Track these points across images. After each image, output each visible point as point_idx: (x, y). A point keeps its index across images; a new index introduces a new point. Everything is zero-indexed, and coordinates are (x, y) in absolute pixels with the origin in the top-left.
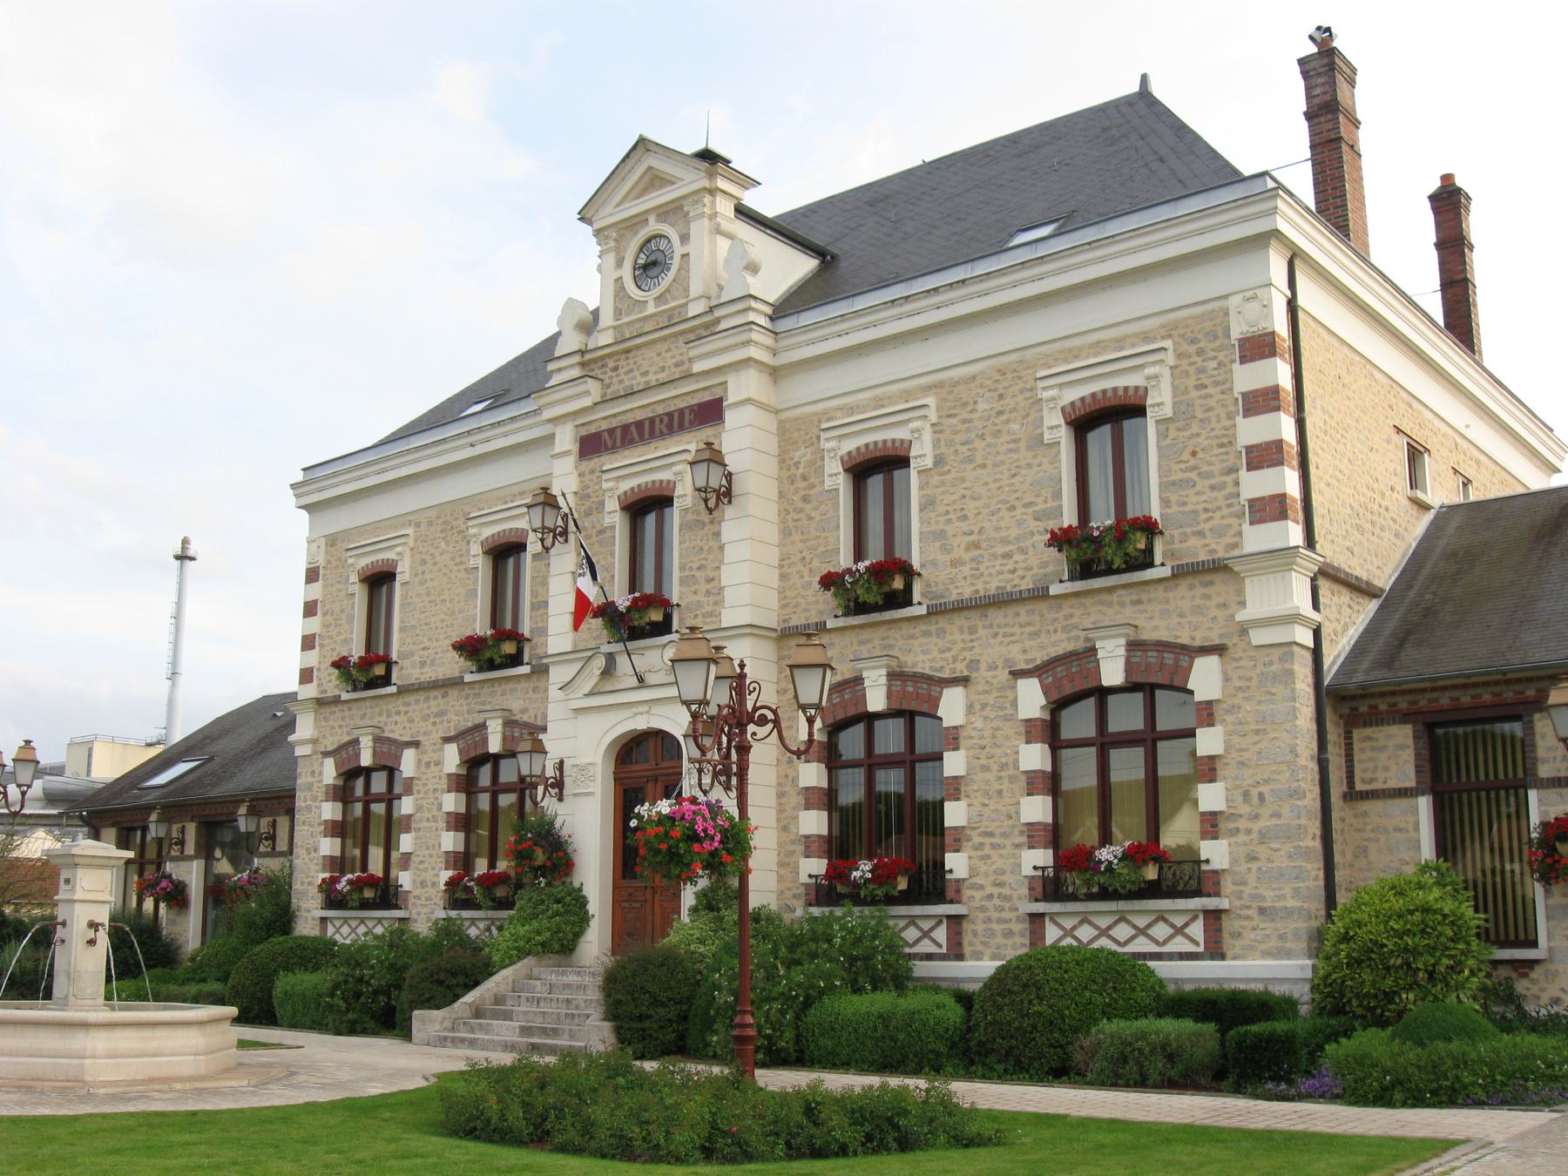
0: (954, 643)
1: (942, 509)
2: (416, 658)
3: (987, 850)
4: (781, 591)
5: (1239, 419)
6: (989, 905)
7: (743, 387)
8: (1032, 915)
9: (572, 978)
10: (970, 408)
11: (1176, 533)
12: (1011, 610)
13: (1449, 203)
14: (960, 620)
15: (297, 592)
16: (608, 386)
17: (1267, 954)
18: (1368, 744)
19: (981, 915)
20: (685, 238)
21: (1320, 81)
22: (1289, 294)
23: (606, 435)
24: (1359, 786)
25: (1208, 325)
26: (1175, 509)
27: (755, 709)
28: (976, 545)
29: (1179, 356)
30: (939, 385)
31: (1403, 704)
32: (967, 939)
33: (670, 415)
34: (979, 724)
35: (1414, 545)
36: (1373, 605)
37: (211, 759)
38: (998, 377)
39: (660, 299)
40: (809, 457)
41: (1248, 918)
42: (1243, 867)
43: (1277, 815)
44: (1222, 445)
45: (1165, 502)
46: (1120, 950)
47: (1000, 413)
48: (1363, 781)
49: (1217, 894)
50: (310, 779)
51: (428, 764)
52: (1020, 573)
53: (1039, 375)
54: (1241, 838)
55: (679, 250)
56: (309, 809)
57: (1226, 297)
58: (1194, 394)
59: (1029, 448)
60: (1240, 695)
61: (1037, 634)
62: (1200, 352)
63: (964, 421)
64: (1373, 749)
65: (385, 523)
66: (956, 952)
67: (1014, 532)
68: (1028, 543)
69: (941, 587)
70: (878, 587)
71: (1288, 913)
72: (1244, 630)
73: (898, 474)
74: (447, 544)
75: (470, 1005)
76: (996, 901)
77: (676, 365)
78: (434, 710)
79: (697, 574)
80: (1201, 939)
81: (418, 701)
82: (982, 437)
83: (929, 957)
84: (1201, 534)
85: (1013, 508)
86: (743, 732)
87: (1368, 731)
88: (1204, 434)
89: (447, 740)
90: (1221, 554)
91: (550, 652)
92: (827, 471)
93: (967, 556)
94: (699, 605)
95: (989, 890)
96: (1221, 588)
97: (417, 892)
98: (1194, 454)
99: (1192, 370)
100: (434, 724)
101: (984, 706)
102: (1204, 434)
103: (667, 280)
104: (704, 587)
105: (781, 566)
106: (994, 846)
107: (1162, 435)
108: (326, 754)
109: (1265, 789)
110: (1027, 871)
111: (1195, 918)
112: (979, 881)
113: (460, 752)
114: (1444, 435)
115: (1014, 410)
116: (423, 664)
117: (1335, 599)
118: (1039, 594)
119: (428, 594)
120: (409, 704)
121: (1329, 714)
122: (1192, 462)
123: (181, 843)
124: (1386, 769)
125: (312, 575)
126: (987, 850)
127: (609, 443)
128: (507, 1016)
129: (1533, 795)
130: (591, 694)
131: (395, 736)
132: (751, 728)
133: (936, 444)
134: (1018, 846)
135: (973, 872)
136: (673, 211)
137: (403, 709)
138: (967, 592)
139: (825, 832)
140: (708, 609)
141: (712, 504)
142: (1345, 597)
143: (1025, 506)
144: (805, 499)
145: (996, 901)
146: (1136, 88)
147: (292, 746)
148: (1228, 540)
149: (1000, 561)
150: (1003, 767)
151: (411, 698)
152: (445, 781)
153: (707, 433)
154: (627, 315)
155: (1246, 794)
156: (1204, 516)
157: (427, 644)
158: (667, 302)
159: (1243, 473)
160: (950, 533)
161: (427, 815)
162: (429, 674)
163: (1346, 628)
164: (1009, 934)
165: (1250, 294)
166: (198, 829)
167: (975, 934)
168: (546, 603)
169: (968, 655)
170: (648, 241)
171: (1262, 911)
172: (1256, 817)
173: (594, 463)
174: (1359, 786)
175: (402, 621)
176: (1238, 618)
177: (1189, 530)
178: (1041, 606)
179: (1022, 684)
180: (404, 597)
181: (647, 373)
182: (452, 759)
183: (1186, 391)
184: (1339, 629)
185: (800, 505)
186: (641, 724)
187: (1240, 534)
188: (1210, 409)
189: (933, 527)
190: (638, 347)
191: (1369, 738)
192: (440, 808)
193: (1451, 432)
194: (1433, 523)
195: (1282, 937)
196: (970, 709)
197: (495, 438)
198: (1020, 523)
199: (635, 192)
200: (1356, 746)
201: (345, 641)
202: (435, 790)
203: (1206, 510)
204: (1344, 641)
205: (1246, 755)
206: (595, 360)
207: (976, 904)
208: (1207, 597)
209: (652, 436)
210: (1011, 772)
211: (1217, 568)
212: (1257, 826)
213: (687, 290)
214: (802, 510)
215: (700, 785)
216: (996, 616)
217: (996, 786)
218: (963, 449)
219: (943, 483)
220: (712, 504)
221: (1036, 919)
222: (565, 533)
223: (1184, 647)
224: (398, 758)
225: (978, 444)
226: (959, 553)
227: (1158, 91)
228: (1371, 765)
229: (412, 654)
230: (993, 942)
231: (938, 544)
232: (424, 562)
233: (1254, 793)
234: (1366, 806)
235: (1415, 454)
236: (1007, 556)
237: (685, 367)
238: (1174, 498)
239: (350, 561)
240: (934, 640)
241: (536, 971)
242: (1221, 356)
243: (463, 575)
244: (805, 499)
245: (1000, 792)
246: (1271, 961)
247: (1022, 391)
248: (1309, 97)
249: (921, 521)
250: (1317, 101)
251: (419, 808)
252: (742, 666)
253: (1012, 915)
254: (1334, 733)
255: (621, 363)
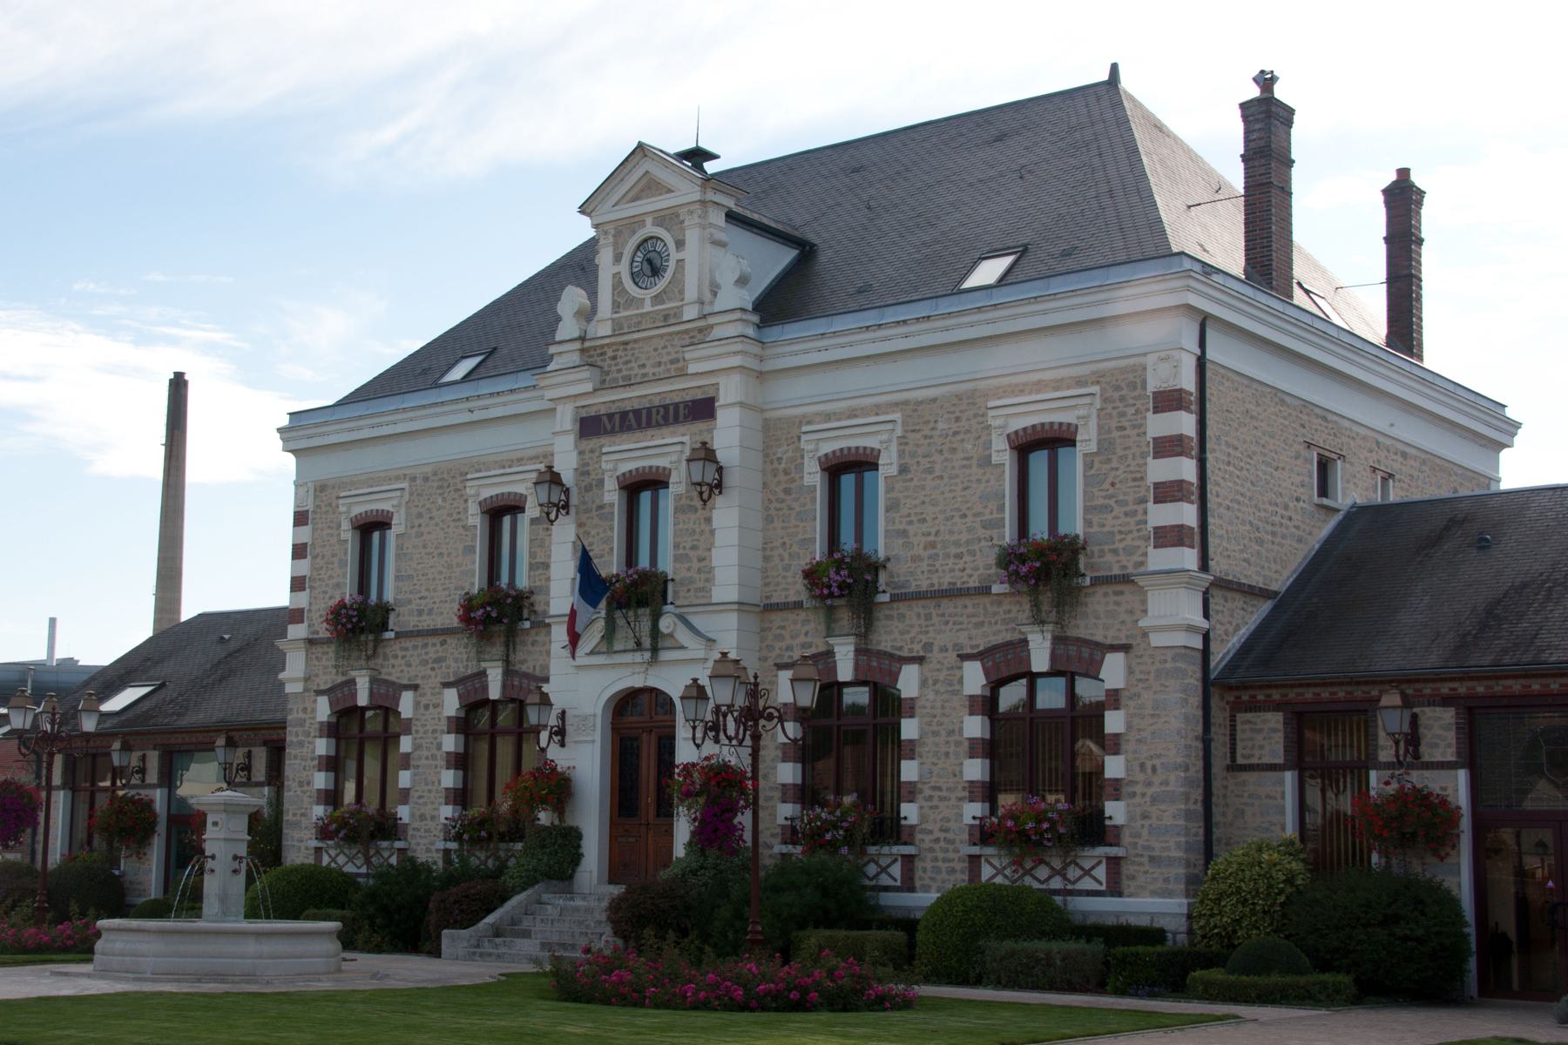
0: (912, 626)
1: (904, 511)
2: (414, 606)
3: (935, 802)
4: (764, 570)
5: (1150, 459)
6: (937, 847)
7: (729, 391)
8: (970, 856)
9: (579, 903)
10: (932, 425)
11: (1096, 549)
12: (960, 602)
13: (1403, 199)
14: (918, 607)
15: (284, 534)
16: (608, 373)
17: (1154, 893)
18: (1247, 727)
19: (930, 856)
20: (680, 244)
21: (1257, 126)
22: (1198, 352)
23: (605, 419)
24: (1240, 761)
25: (1131, 377)
26: (1095, 529)
27: (765, 708)
28: (933, 545)
29: (1105, 400)
30: (906, 403)
31: (1276, 695)
32: (919, 873)
33: (666, 407)
34: (931, 696)
35: (1317, 546)
36: (1266, 607)
37: (163, 685)
38: (955, 401)
39: (657, 299)
40: (790, 454)
41: (1140, 864)
42: (1139, 823)
43: (1166, 783)
44: (1135, 480)
45: (1088, 523)
46: (1044, 887)
47: (956, 433)
48: (1243, 756)
49: (1117, 845)
50: (301, 715)
51: (427, 707)
52: (968, 571)
53: (990, 404)
54: (1137, 800)
55: (674, 256)
56: (301, 744)
57: (1145, 354)
58: (1116, 434)
59: (979, 466)
60: (1141, 685)
61: (980, 624)
62: (1122, 399)
63: (926, 437)
64: (1252, 730)
65: (379, 472)
66: (908, 885)
67: (964, 537)
68: (976, 547)
69: (902, 578)
70: (848, 583)
71: (1171, 861)
72: (1145, 635)
73: (868, 475)
74: (444, 500)
75: (492, 925)
76: (942, 844)
77: (672, 362)
78: (433, 655)
79: (691, 553)
80: (1103, 879)
81: (415, 647)
82: (941, 452)
83: (887, 889)
84: (1115, 552)
85: (965, 516)
86: (756, 725)
87: (1249, 716)
88: (1122, 468)
89: (447, 685)
90: (1130, 571)
91: (552, 612)
92: (806, 469)
93: (925, 554)
94: (692, 581)
95: (937, 834)
96: (1129, 598)
97: (416, 825)
98: (1113, 484)
99: (1115, 413)
100: (433, 669)
101: (935, 682)
102: (1122, 468)
103: (662, 284)
104: (696, 565)
105: (764, 549)
106: (941, 799)
107: (1089, 466)
108: (320, 693)
109: (1157, 762)
110: (968, 820)
111: (1099, 863)
112: (929, 827)
113: (460, 697)
114: (1364, 438)
115: (968, 431)
116: (420, 613)
117: (1229, 605)
118: (984, 591)
119: (425, 547)
120: (406, 649)
121: (1215, 702)
122: (1112, 490)
123: (142, 771)
124: (1261, 747)
125: (300, 519)
126: (935, 802)
127: (609, 427)
128: (526, 934)
129: (1373, 774)
130: (592, 653)
131: (393, 678)
132: (762, 722)
133: (901, 454)
134: (960, 799)
135: (923, 818)
136: (668, 218)
137: (400, 654)
138: (924, 586)
139: (799, 781)
140: (700, 585)
141: (705, 496)
142: (1238, 601)
143: (975, 515)
144: (787, 491)
145: (942, 844)
146: (1105, 77)
147: (282, 684)
148: (1136, 558)
149: (952, 560)
150: (950, 733)
151: (408, 643)
152: (444, 723)
153: (700, 426)
154: (626, 309)
155: (1142, 766)
156: (1118, 537)
157: (424, 593)
158: (663, 302)
159: (1150, 505)
160: (911, 533)
161: (425, 753)
162: (427, 622)
163: (1237, 628)
164: (952, 871)
165: (1163, 355)
166: (161, 757)
167: (924, 870)
168: (546, 566)
169: (924, 638)
170: (646, 241)
171: (1152, 859)
172: (1149, 784)
173: (593, 443)
174: (1240, 761)
175: (398, 570)
176: (1141, 624)
177: (1106, 548)
178: (986, 600)
179: (967, 664)
180: (399, 547)
181: (644, 366)
182: (451, 702)
183: (1109, 431)
184: (1231, 629)
185: (782, 496)
186: (638, 682)
187: (1146, 554)
188: (1129, 448)
189: (898, 526)
190: (636, 341)
191: (1249, 722)
192: (439, 746)
193: (1370, 433)
194: (1340, 523)
195: (1166, 880)
196: (923, 683)
197: (495, 405)
198: (969, 530)
199: (630, 195)
200: (1239, 727)
201: (338, 585)
202: (434, 731)
203: (1120, 532)
204: (1235, 639)
205: (1144, 734)
206: (595, 348)
207: (926, 845)
208: (1118, 604)
209: (649, 425)
210: (957, 738)
211: (1126, 579)
212: (1150, 791)
213: (682, 292)
214: (783, 501)
215: (694, 739)
216: (948, 606)
217: (944, 749)
218: (924, 461)
219: (907, 489)
220: (705, 496)
221: (974, 860)
222: (566, 506)
223: (1097, 644)
224: (397, 700)
225: (938, 458)
226: (919, 551)
227: (1126, 83)
228: (1250, 744)
229: (410, 602)
230: (939, 877)
231: (901, 541)
232: (420, 515)
233: (1149, 764)
234: (1245, 776)
235: (1324, 466)
236: (959, 556)
237: (680, 364)
238: (1095, 520)
239: (343, 509)
240: (896, 623)
241: (545, 897)
242: (1139, 403)
243: (461, 531)
244: (787, 491)
245: (947, 754)
246: (1157, 903)
247: (976, 416)
248: (1247, 140)
249: (887, 520)
250: (1253, 145)
251: (417, 747)
252: (756, 677)
253: (955, 856)
254: (1219, 716)
255: (620, 353)
